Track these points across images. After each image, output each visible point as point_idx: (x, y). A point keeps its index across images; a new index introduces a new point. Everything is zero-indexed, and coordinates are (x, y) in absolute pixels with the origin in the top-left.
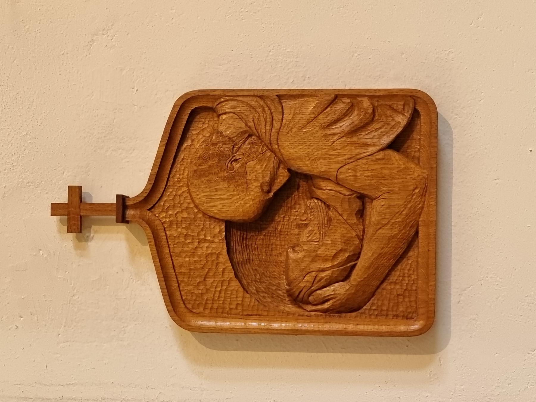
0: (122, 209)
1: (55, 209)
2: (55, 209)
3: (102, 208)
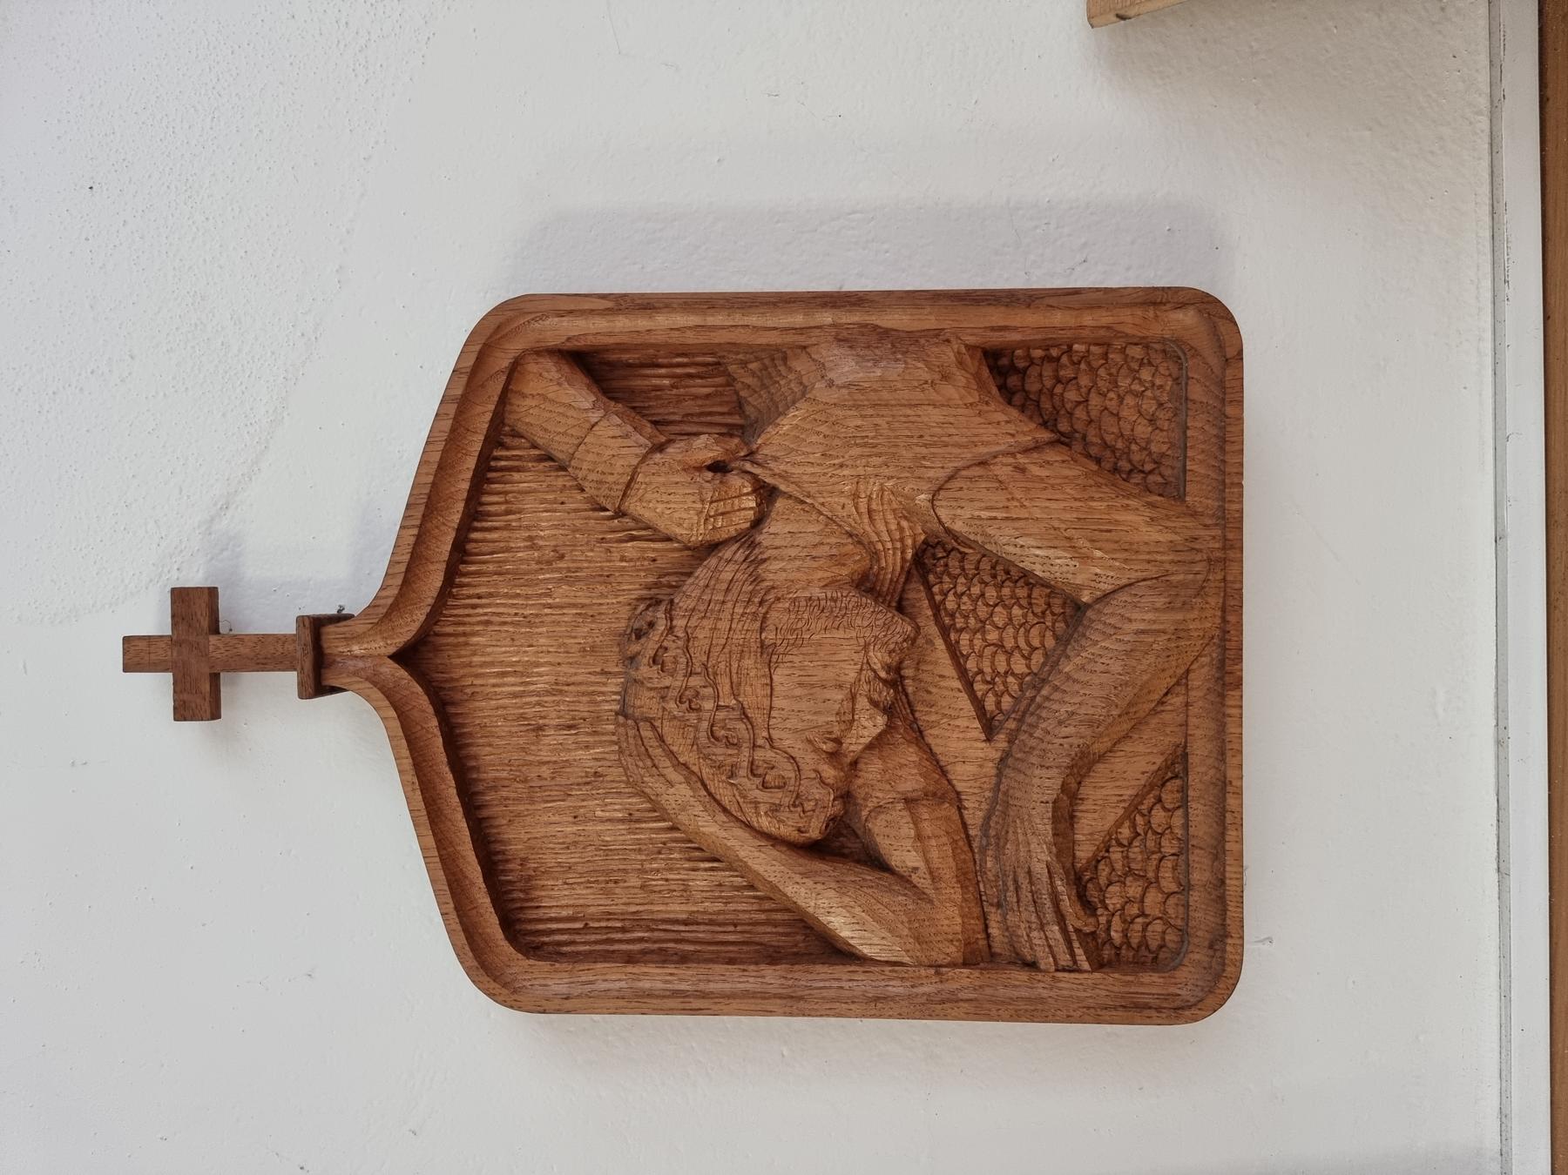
0: (316, 657)
1: (138, 654)
2: (138, 655)
3: (264, 654)
